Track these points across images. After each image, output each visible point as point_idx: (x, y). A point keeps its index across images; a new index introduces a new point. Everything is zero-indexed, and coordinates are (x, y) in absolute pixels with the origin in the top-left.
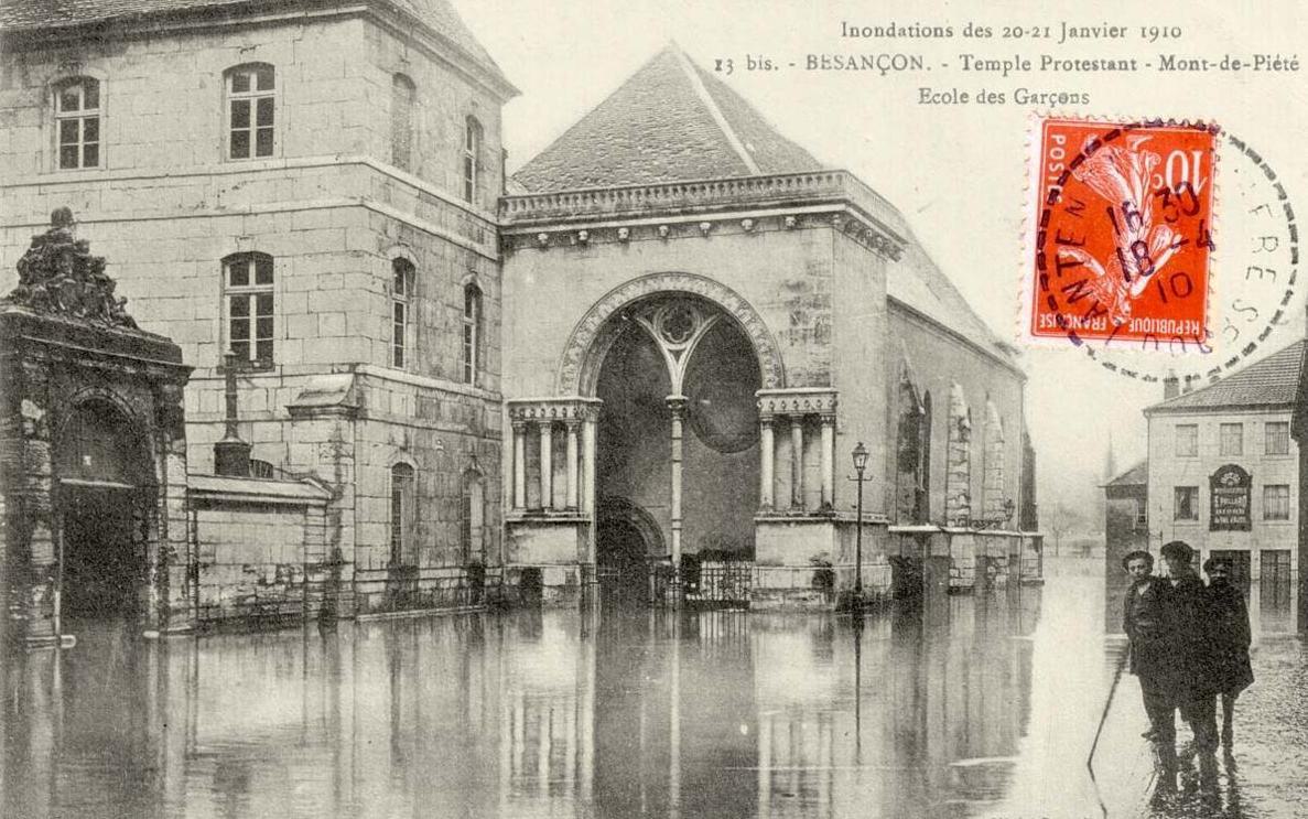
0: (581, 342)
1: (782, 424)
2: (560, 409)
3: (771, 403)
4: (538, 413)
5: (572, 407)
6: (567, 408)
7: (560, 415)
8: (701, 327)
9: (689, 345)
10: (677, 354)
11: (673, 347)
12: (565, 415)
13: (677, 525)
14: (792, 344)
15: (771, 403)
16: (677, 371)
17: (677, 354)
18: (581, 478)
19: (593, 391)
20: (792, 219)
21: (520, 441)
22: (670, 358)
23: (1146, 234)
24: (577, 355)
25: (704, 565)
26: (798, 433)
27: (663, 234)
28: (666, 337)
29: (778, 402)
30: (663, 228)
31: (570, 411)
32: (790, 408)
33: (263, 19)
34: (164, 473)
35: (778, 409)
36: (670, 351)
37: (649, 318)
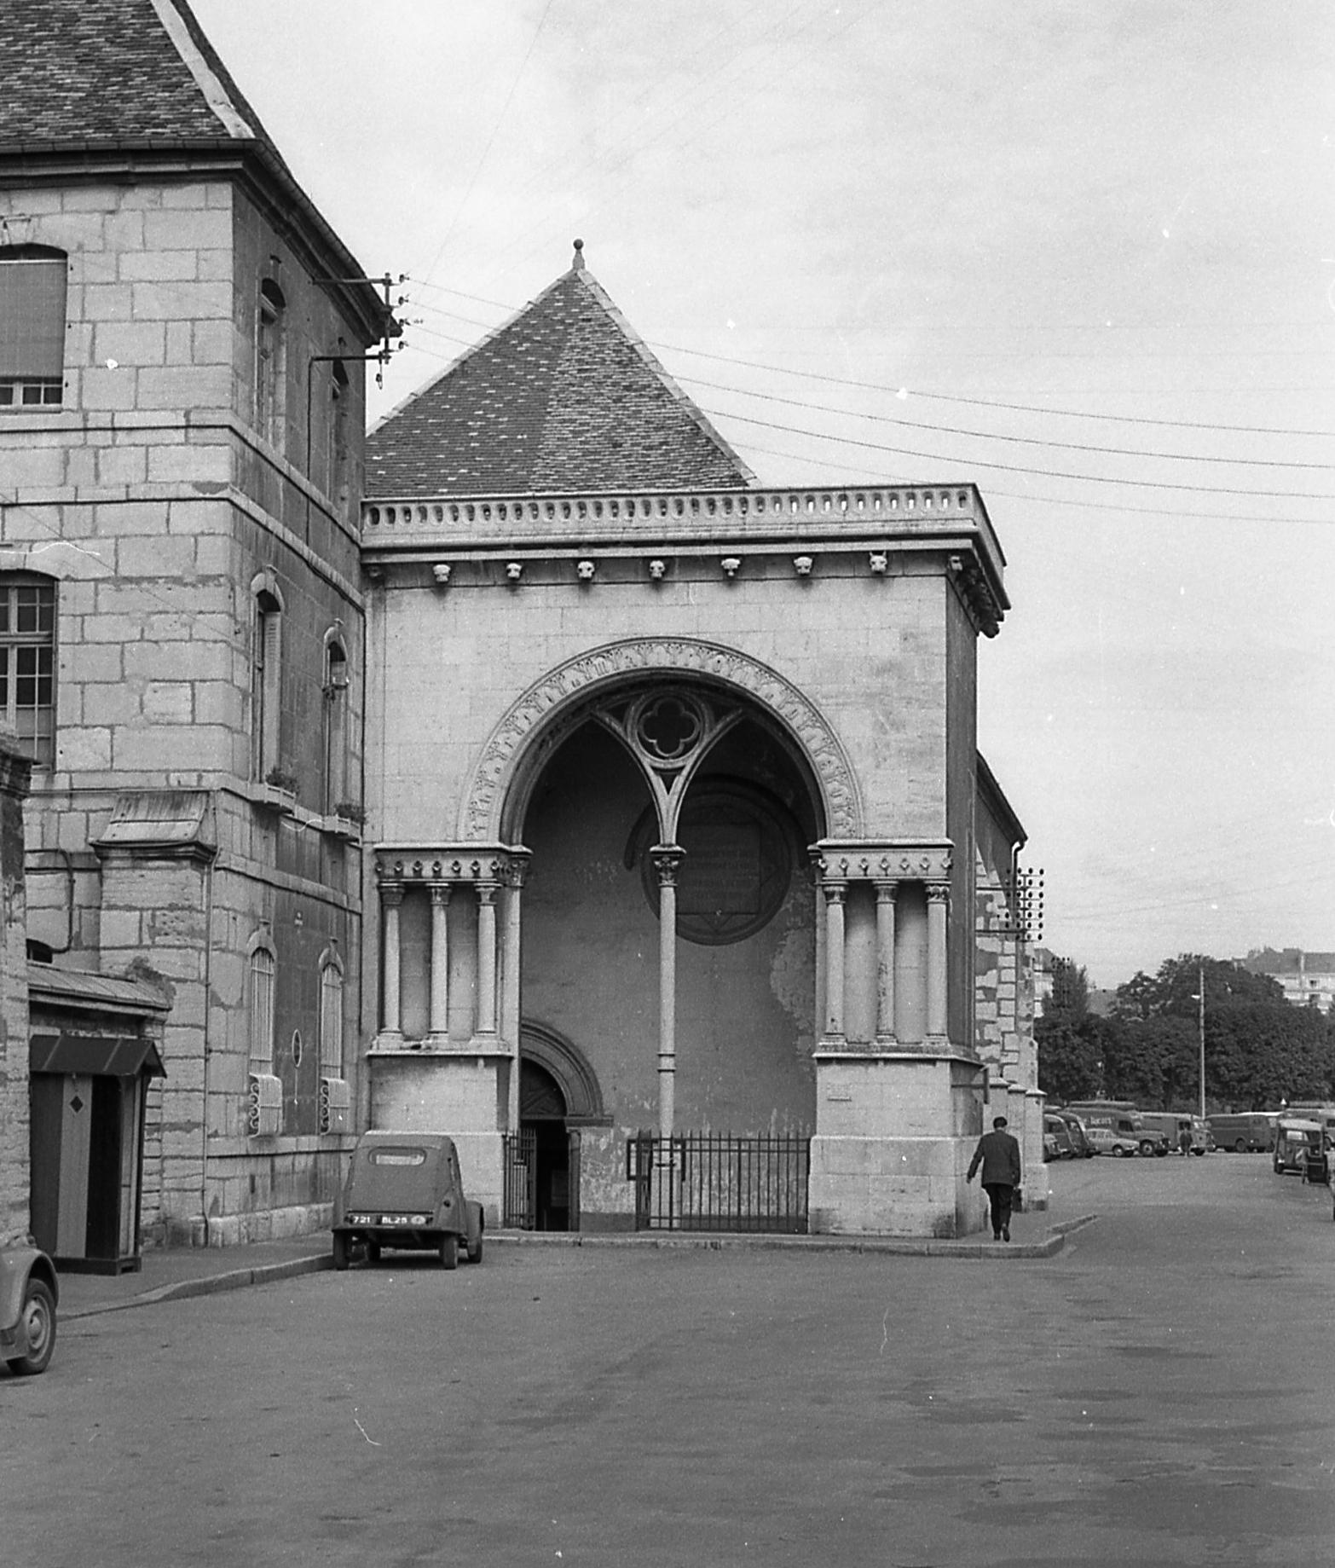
0: (506, 750)
1: (860, 894)
2: (466, 865)
3: (844, 861)
4: (427, 871)
5: (490, 861)
6: (481, 861)
7: (466, 873)
8: (708, 735)
9: (688, 762)
10: (668, 777)
11: (660, 764)
12: (476, 873)
13: (667, 1063)
14: (877, 767)
15: (844, 861)
16: (668, 803)
17: (668, 777)
18: (499, 969)
19: (518, 835)
20: (589, 564)
21: (393, 916)
22: (657, 782)
23: (120, 853)
24: (497, 770)
25: (554, 1204)
26: (887, 910)
27: (657, 574)
28: (650, 749)
29: (854, 860)
30: (657, 565)
31: (486, 865)
32: (874, 872)
33: (310, 246)
34: (118, 869)
35: (855, 873)
36: (654, 769)
37: (619, 714)
